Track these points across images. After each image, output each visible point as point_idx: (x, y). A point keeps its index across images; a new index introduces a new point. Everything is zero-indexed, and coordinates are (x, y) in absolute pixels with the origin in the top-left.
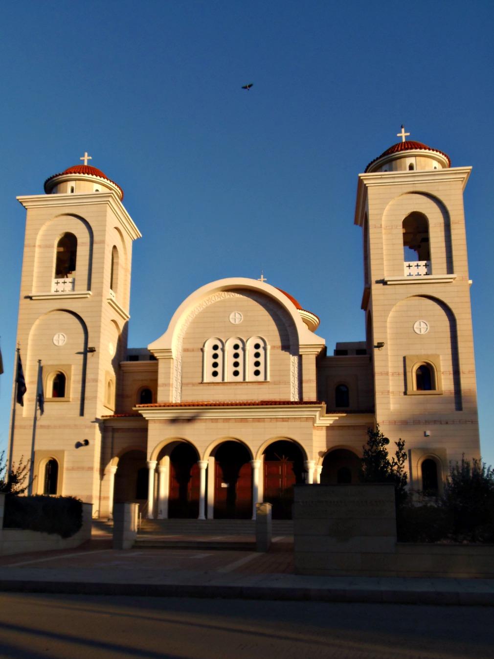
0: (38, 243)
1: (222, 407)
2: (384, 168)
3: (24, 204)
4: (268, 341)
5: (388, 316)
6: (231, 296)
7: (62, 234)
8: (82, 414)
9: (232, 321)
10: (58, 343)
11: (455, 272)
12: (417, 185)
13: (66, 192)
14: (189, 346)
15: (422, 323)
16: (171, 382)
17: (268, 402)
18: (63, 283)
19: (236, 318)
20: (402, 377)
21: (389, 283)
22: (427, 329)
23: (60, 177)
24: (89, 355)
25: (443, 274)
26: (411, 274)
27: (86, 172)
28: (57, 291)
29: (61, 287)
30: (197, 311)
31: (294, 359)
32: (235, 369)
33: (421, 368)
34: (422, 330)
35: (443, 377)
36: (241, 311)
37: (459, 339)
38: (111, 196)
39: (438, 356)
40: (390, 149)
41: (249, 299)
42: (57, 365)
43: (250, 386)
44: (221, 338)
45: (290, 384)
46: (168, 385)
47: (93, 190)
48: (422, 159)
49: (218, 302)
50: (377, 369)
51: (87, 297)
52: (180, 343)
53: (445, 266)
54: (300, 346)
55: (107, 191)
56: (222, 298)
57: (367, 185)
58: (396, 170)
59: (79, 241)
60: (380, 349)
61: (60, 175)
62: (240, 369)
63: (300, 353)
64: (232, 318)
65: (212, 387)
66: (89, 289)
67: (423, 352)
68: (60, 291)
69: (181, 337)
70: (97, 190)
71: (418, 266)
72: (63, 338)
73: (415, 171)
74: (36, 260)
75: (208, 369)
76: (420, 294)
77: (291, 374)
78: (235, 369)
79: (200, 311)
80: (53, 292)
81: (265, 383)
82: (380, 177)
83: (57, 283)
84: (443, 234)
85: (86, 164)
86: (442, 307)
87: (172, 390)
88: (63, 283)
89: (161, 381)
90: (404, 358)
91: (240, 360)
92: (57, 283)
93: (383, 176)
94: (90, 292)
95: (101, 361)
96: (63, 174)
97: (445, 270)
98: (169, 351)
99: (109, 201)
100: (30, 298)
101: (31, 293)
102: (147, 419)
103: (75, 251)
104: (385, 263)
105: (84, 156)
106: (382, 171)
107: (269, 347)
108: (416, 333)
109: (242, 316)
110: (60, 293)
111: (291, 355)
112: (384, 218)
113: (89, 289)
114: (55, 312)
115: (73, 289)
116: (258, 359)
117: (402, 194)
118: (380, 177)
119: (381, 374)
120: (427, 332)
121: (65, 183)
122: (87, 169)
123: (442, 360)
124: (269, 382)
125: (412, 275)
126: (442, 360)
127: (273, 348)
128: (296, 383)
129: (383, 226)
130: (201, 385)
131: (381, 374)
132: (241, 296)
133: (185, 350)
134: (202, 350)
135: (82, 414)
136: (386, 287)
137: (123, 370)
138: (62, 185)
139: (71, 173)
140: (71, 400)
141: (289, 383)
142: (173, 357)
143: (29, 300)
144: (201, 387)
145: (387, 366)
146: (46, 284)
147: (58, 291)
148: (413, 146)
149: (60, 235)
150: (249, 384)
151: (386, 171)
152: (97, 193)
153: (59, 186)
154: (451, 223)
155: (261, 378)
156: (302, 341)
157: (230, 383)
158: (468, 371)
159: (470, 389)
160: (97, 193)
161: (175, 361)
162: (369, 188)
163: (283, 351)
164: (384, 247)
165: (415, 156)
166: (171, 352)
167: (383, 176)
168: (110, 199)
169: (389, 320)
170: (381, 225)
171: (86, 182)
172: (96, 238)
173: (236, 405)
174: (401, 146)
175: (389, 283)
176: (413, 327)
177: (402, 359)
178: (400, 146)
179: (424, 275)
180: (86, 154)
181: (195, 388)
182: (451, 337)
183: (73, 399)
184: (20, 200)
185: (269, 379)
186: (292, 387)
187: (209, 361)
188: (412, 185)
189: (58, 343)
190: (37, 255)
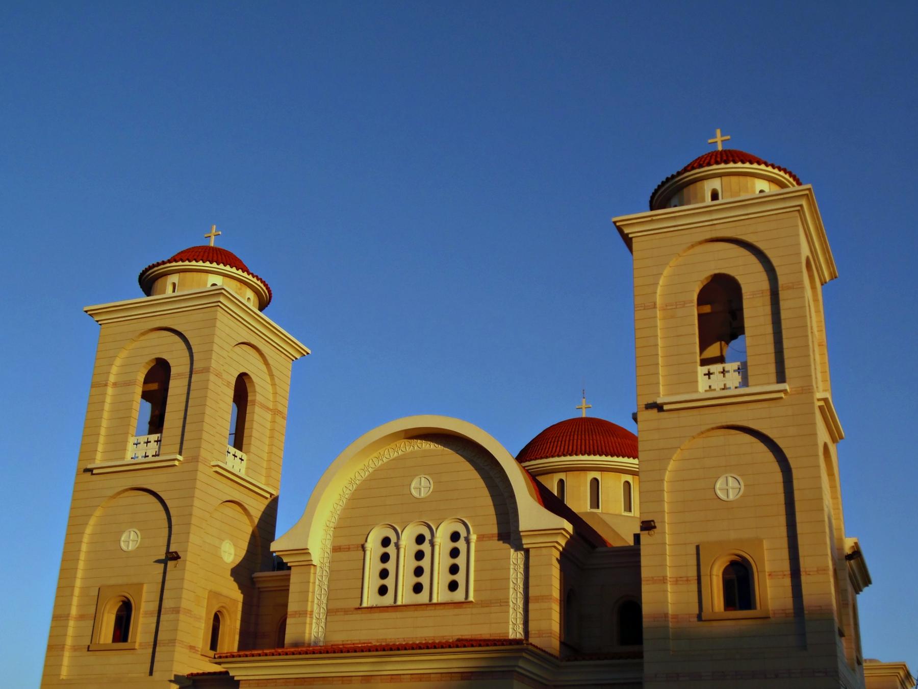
0: (112, 379)
1: (285, 657)
2: (675, 200)
3: (626, 231)
4: (472, 526)
5: (666, 469)
6: (416, 448)
7: (707, 278)
8: (151, 673)
9: (415, 493)
10: (728, 497)
11: (787, 380)
12: (717, 227)
13: (703, 200)
14: (343, 542)
15: (730, 479)
16: (309, 609)
17: (499, 640)
18: (155, 441)
19: (421, 487)
20: (695, 587)
21: (665, 407)
22: (740, 488)
23: (156, 269)
24: (171, 564)
25: (769, 384)
26: (713, 388)
27: (721, 159)
28: (146, 456)
29: (717, 381)
30: (360, 478)
31: (516, 558)
32: (417, 580)
33: (733, 564)
34: (731, 491)
35: (768, 582)
36: (429, 474)
37: (798, 506)
38: (222, 293)
39: (760, 541)
40: (688, 166)
41: (447, 450)
42: (121, 585)
43: (440, 612)
44: (393, 525)
45: (509, 606)
46: (303, 613)
47: (206, 284)
48: (734, 179)
49: (393, 460)
50: (645, 573)
51: (174, 465)
52: (328, 537)
53: (772, 368)
54: (522, 534)
55: (775, 189)
56: (400, 452)
57: (630, 236)
58: (689, 203)
59: (174, 371)
60: (652, 532)
61: (164, 263)
62: (424, 580)
63: (525, 546)
64: (415, 488)
65: (376, 615)
66: (781, 377)
67: (733, 535)
68: (150, 456)
69: (332, 525)
70: (214, 285)
71: (148, 442)
72: (737, 485)
73: (720, 201)
74: (107, 407)
75: (372, 582)
76: (724, 424)
77: (511, 585)
78: (417, 580)
79: (364, 477)
80: (128, 459)
81: (464, 605)
82: (649, 219)
83: (709, 374)
84: (768, 309)
85: (720, 148)
86: (768, 448)
87: (311, 624)
88: (155, 441)
89: (292, 607)
90: (698, 547)
91: (390, 566)
92: (709, 374)
93: (654, 218)
94: (785, 386)
95: (188, 575)
96: (169, 261)
97: (773, 377)
98: (305, 552)
99: (220, 302)
100: (659, 408)
101: (94, 463)
102: (236, 678)
103: (741, 309)
104: (661, 371)
105: (714, 136)
106: (670, 207)
107: (473, 537)
108: (719, 498)
109: (432, 482)
110: (150, 459)
111: (512, 551)
112: (659, 290)
113: (781, 377)
114: (126, 494)
115: (745, 383)
116: (421, 563)
117: (693, 246)
118: (649, 219)
119: (653, 580)
120: (738, 497)
121: (691, 187)
122: (215, 251)
123: (767, 549)
124: (471, 602)
125: (730, 388)
126: (767, 549)
127: (481, 538)
128: (520, 603)
129: (658, 305)
130: (359, 611)
131: (653, 580)
132: (440, 447)
133: (336, 549)
134: (363, 548)
135: (151, 673)
136: (662, 414)
137: (259, 588)
138: (159, 282)
139: (709, 164)
140: (137, 646)
141: (506, 603)
142: (314, 563)
143: (655, 411)
144: (357, 616)
145: (663, 566)
146: (117, 444)
147: (148, 456)
148: (737, 159)
149: (702, 282)
150: (438, 607)
151: (675, 206)
152: (762, 195)
153: (156, 283)
154: (780, 289)
155: (459, 595)
156: (523, 526)
157: (371, 608)
158: (815, 569)
159: (820, 606)
160: (762, 195)
161: (318, 569)
162: (634, 240)
163: (501, 542)
164: (660, 342)
165: (720, 175)
166: (309, 553)
167: (654, 218)
168: (222, 299)
169: (667, 476)
170: (655, 304)
171: (195, 273)
172: (782, 281)
173: (369, 649)
174: (716, 156)
175: (665, 407)
176: (714, 488)
177: (694, 551)
178: (714, 157)
179: (153, 456)
180: (718, 132)
181: (347, 617)
182: (785, 504)
183: (141, 644)
184: (618, 224)
185: (471, 598)
186: (511, 611)
187: (372, 566)
188: (709, 228)
189: (728, 497)
190: (108, 400)
